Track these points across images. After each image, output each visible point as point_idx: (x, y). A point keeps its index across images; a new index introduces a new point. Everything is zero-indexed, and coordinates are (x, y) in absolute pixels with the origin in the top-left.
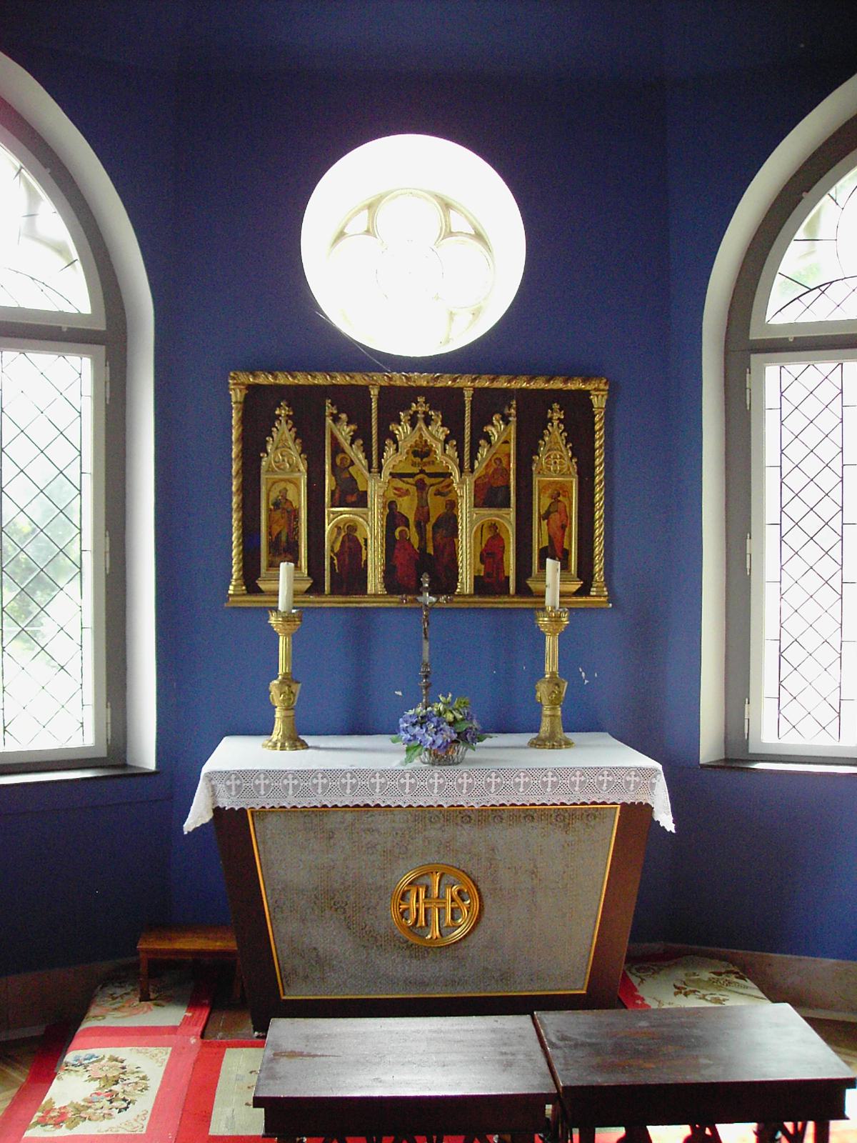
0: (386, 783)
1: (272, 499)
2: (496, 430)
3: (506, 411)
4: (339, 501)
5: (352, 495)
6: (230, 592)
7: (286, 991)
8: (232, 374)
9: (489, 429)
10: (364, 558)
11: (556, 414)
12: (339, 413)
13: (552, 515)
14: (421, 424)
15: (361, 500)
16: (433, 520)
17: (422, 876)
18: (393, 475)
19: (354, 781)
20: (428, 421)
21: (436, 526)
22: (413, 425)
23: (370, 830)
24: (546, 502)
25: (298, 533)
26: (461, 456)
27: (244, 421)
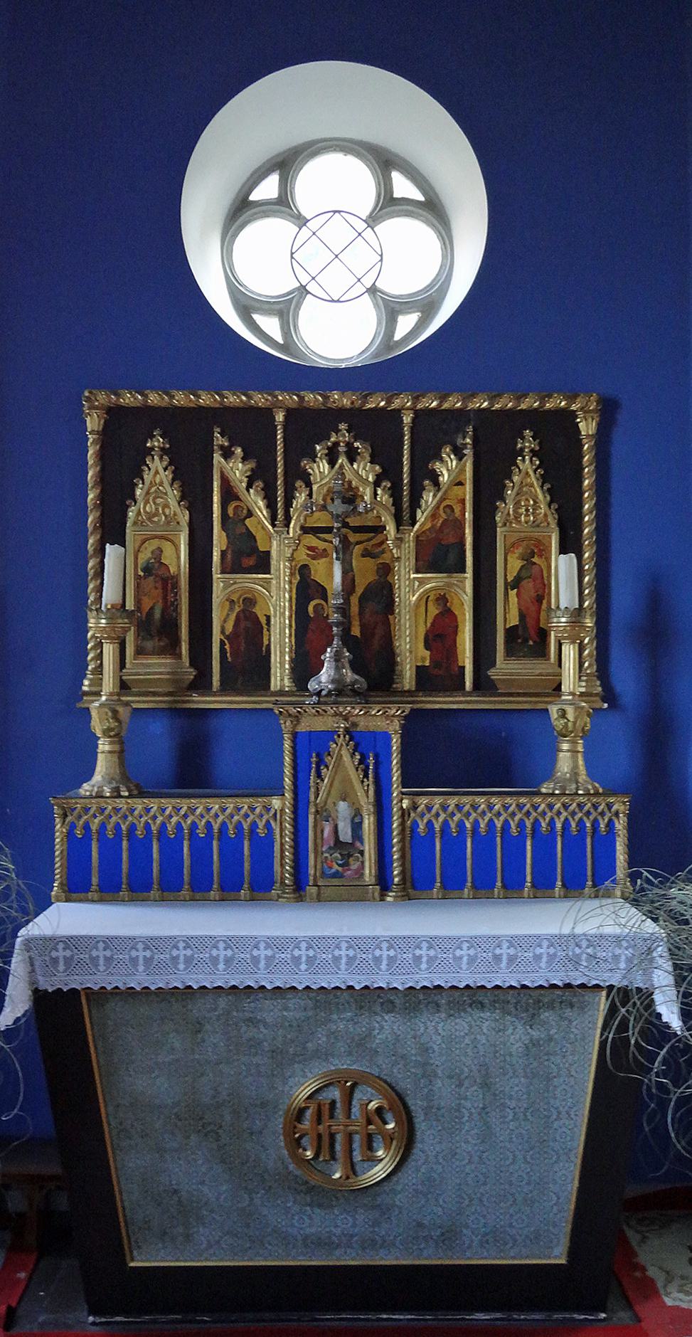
0: (273, 957)
1: (140, 562)
2: (447, 468)
3: (460, 441)
4: (233, 566)
5: (249, 555)
6: (85, 688)
7: (135, 1253)
8: (87, 394)
9: (438, 466)
10: (266, 642)
11: (528, 442)
12: (231, 446)
13: (524, 583)
14: (342, 460)
15: (263, 563)
16: (359, 590)
17: (325, 1086)
18: (305, 530)
19: (229, 953)
20: (352, 456)
21: (362, 599)
22: (332, 463)
23: (251, 1021)
24: (515, 564)
25: (176, 609)
26: (397, 503)
27: (102, 456)
